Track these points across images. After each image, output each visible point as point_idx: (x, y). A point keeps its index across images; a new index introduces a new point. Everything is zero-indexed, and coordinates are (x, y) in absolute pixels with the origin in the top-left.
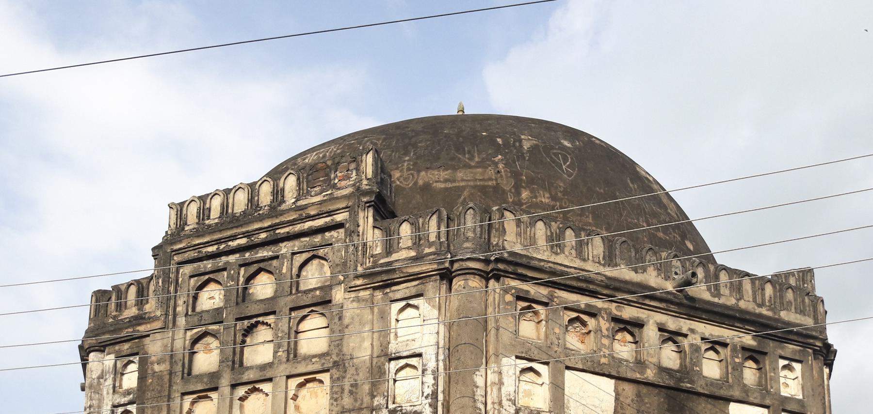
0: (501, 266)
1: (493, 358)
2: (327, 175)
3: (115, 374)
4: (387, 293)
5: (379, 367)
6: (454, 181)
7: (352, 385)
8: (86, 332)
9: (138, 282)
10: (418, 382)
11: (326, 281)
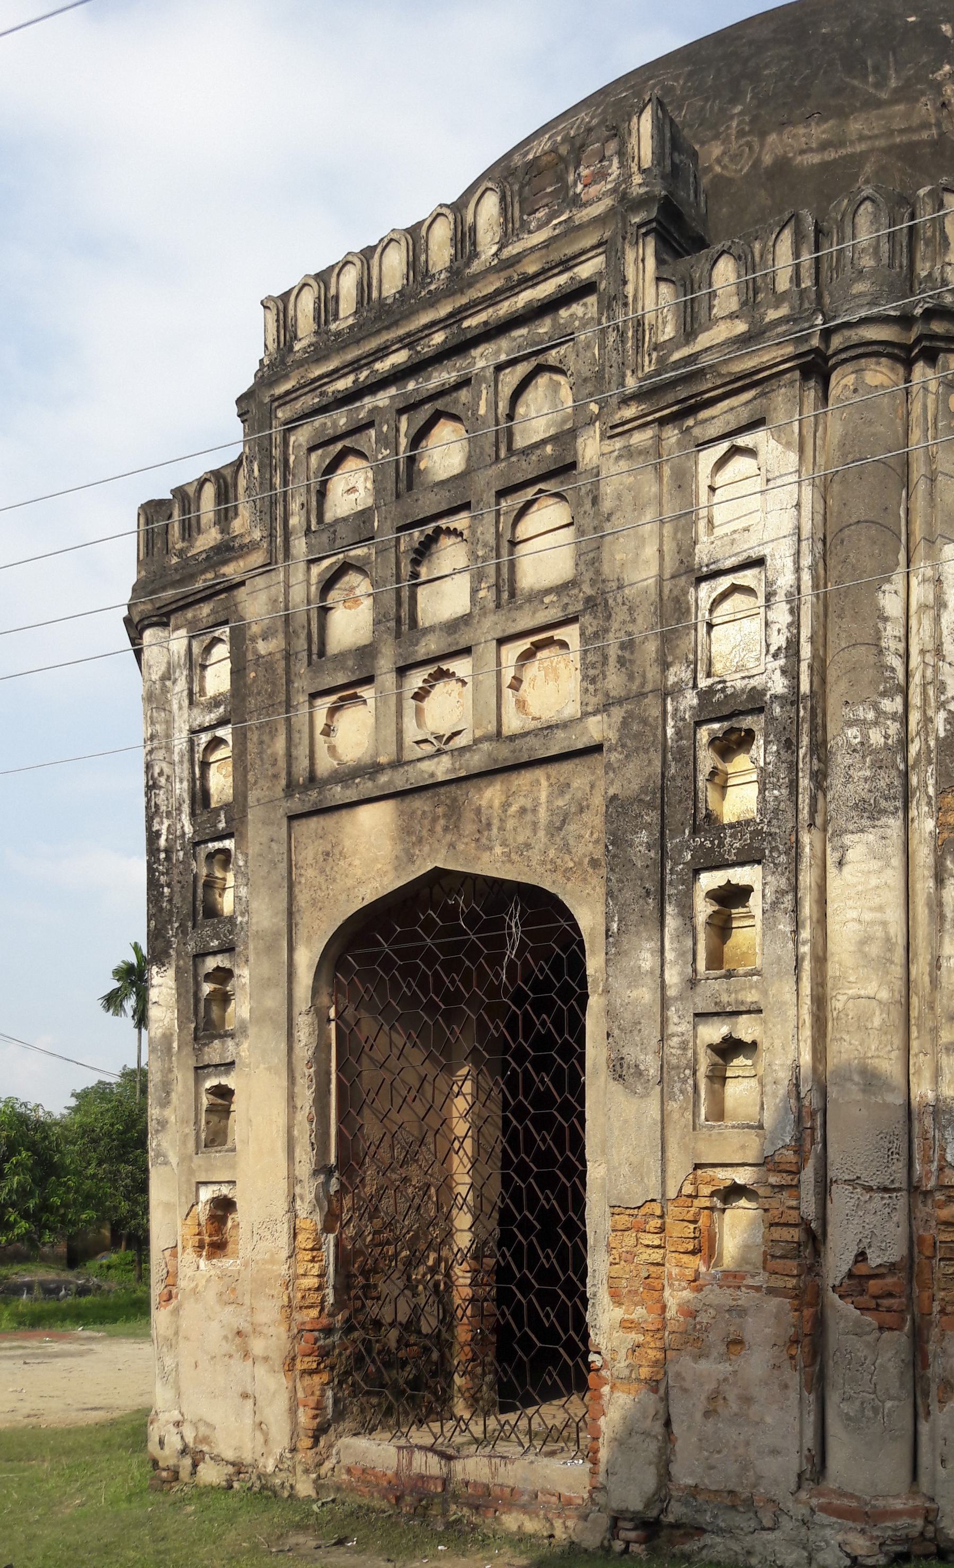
0: (938, 327)
1: (921, 550)
2: (561, 178)
3: (191, 669)
4: (689, 428)
5: (677, 600)
6: (842, 144)
7: (623, 646)
8: (134, 590)
9: (217, 475)
10: (754, 626)
11: (564, 422)
